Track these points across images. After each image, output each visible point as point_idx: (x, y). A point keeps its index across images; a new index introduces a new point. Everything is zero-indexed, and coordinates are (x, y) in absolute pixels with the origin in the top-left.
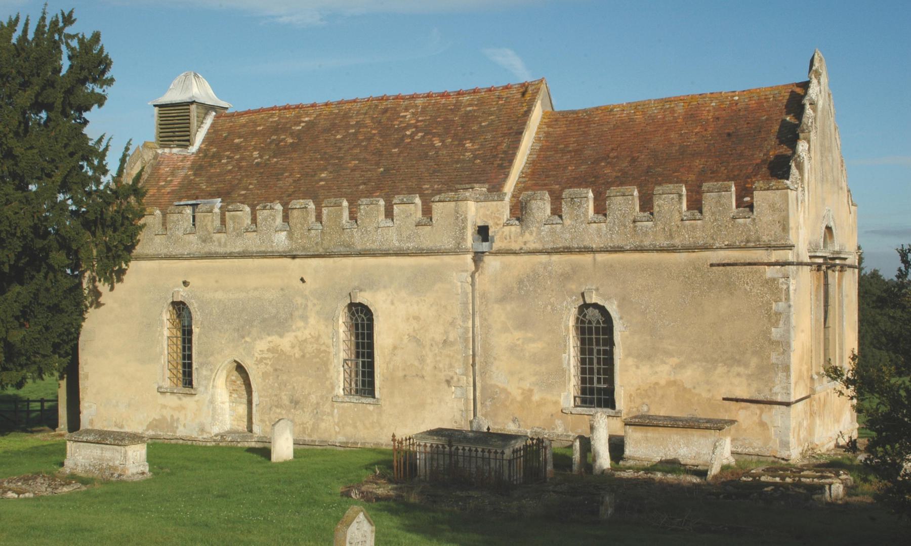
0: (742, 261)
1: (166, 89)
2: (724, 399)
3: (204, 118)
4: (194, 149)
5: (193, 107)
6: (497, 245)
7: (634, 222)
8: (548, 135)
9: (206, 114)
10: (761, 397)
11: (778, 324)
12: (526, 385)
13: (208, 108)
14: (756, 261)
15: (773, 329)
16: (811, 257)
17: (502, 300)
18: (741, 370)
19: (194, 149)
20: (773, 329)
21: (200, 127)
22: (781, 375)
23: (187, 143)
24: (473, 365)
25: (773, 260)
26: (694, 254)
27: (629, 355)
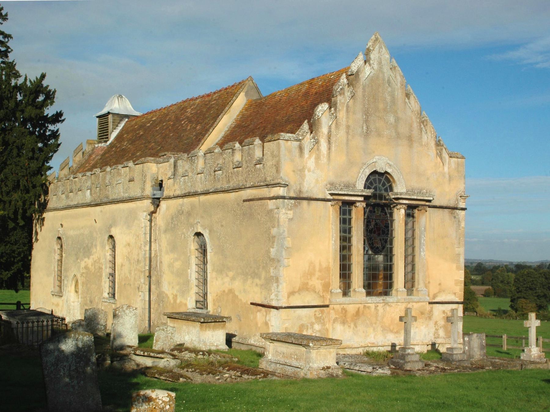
0: (257, 197)
1: (103, 106)
2: (252, 304)
3: (119, 123)
4: (108, 143)
5: (110, 116)
6: (166, 193)
7: (215, 171)
8: (243, 115)
9: (121, 120)
10: (265, 303)
11: (273, 245)
12: (175, 292)
13: (122, 117)
14: (263, 196)
15: (272, 249)
16: (332, 194)
17: (165, 231)
18: (257, 281)
19: (108, 143)
20: (272, 249)
21: (115, 129)
22: (275, 285)
23: (106, 139)
24: (150, 277)
25: (272, 195)
26: (237, 193)
27: (213, 270)
